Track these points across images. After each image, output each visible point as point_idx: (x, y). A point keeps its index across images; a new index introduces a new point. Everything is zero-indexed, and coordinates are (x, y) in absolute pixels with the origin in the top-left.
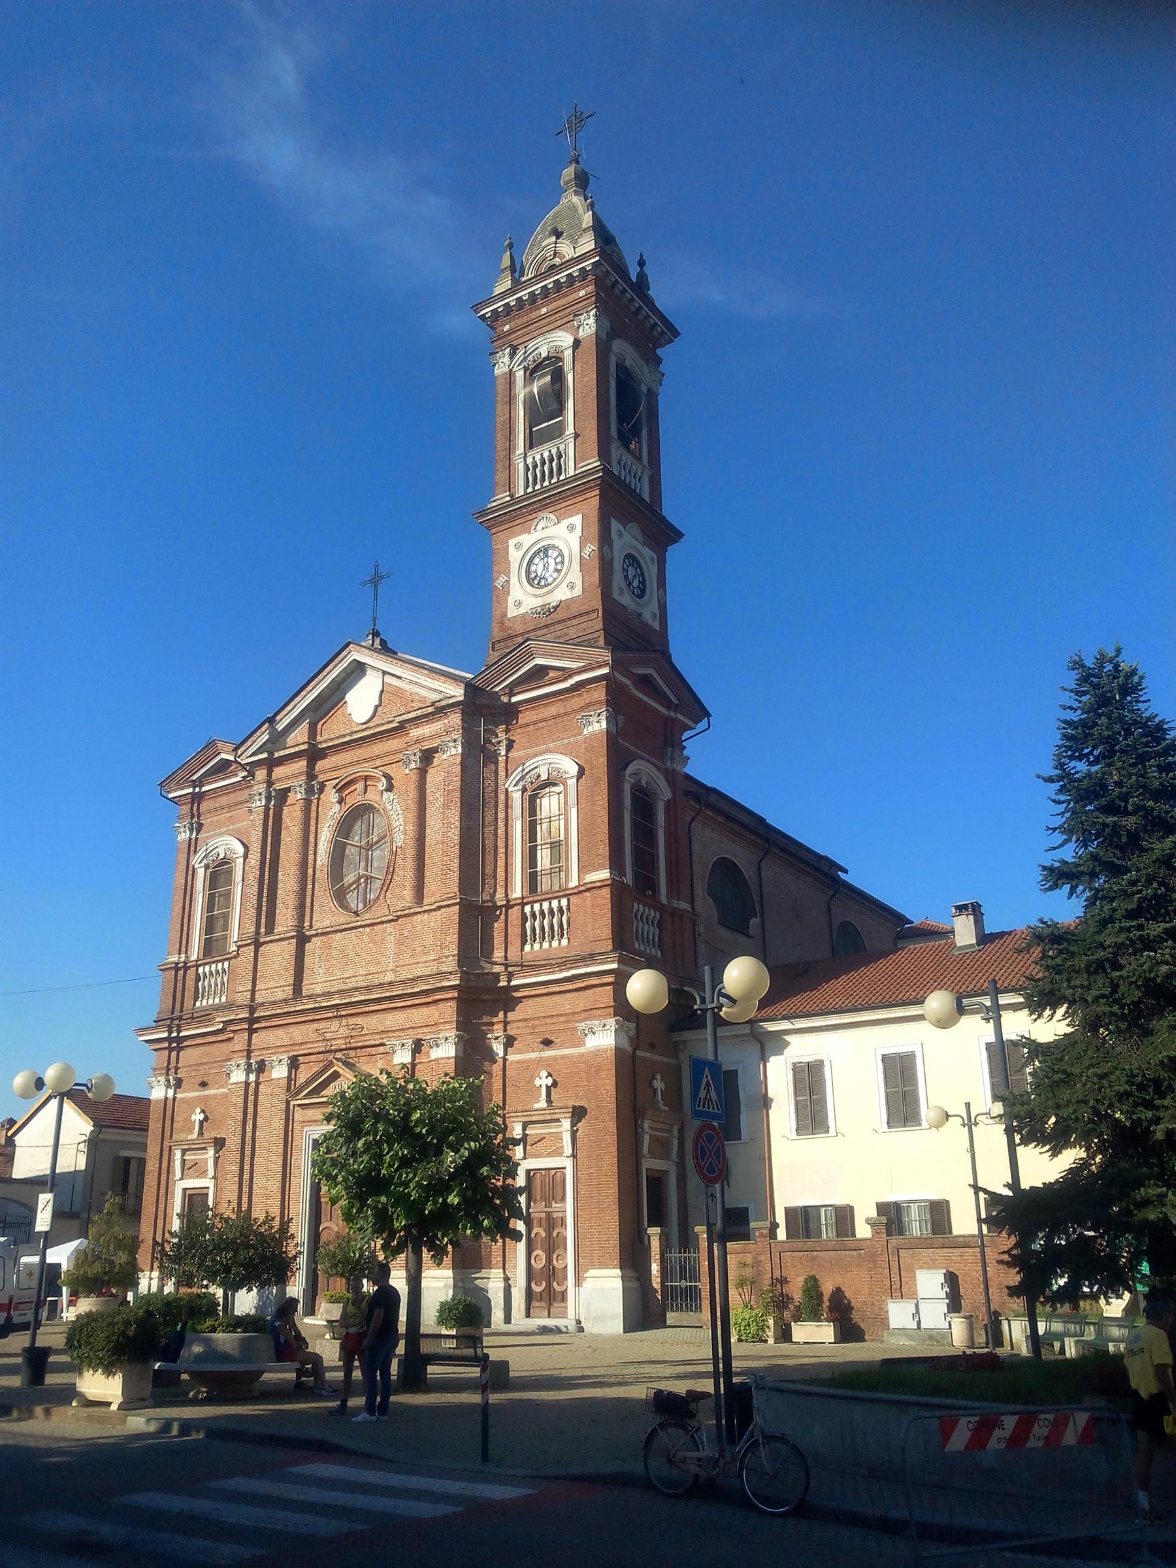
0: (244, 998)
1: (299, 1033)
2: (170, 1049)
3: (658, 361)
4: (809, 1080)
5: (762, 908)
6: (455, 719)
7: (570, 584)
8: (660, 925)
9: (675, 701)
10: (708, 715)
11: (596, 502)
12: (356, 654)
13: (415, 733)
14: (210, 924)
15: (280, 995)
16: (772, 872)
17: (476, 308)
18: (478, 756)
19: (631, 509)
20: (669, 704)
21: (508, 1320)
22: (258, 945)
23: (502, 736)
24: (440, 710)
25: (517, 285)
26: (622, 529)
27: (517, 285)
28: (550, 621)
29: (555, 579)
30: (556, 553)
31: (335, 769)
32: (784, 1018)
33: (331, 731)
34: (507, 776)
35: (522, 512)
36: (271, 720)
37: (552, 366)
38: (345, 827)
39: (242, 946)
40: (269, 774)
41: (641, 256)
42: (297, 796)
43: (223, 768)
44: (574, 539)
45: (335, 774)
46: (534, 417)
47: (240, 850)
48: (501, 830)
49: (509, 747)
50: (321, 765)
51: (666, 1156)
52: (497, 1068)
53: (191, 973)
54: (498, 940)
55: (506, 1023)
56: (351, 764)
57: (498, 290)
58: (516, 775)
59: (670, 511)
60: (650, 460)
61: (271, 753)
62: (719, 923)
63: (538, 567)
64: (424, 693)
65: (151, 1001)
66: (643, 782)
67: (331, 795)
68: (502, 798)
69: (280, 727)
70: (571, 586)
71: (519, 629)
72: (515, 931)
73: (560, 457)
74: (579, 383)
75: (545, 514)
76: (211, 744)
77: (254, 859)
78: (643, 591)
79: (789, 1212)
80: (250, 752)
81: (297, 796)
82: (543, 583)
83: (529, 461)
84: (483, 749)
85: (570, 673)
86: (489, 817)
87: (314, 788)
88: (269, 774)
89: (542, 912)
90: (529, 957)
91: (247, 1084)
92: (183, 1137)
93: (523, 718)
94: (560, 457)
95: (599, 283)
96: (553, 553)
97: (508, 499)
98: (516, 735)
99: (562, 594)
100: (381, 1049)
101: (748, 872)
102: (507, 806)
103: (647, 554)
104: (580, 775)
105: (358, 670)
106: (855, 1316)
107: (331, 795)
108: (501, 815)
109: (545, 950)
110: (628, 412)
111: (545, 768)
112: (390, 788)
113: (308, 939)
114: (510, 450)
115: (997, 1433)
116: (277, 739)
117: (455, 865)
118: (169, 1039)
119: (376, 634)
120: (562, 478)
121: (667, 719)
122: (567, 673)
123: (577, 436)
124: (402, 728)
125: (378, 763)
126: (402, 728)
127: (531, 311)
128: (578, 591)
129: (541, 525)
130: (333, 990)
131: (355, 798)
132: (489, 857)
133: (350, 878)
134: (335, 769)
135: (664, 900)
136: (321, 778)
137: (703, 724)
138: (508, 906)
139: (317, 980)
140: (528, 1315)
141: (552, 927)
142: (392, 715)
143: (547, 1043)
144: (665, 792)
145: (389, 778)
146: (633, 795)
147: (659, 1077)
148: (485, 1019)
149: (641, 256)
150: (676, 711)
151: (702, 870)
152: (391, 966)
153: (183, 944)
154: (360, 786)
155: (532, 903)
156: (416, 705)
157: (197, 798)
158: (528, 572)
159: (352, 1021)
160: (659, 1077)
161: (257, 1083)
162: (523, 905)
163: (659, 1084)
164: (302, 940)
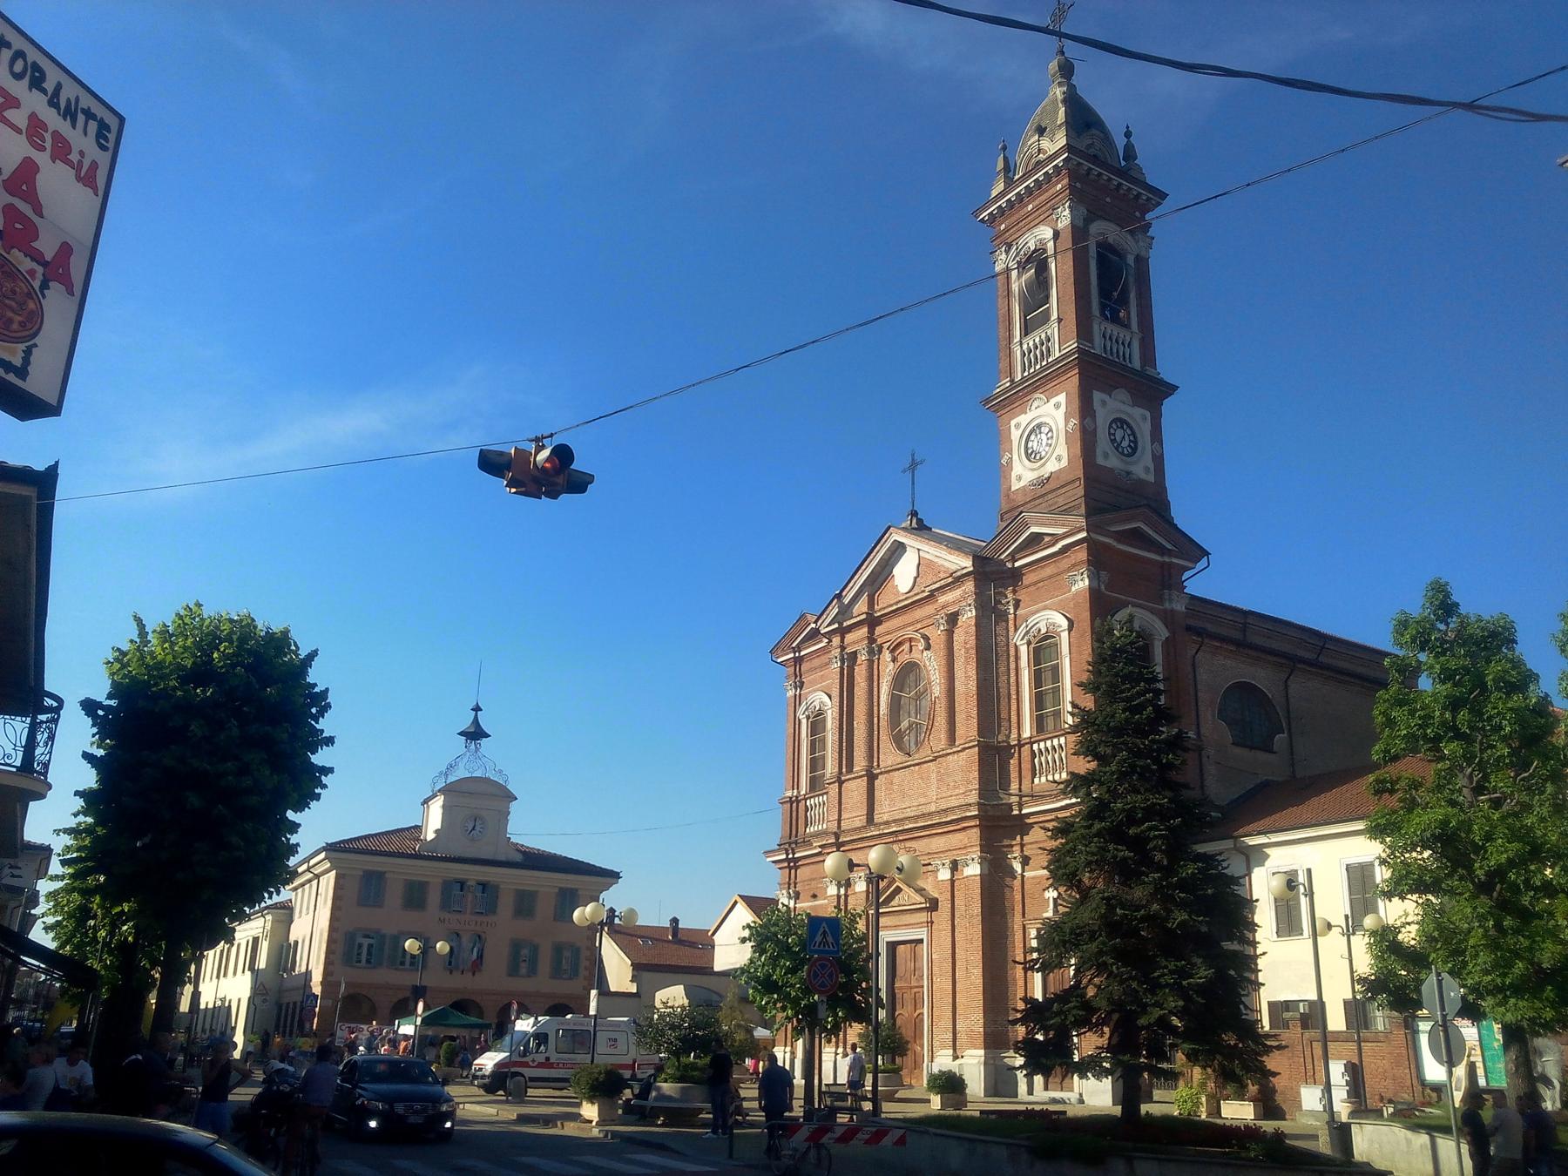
0: (833, 826)
2: (790, 868)
4: (1292, 886)
5: (1289, 724)
6: (969, 586)
7: (1058, 456)
9: (1169, 546)
10: (1208, 554)
11: (1076, 379)
12: (897, 536)
13: (942, 599)
14: (1039, 701)
15: (858, 824)
16: (1304, 688)
17: (976, 213)
18: (991, 617)
19: (1120, 377)
20: (1162, 550)
21: (1030, 1092)
22: (841, 783)
23: (1010, 596)
24: (958, 580)
25: (1010, 183)
27: (1010, 183)
28: (1044, 488)
31: (888, 633)
32: (1260, 833)
33: (885, 602)
34: (1016, 630)
35: (1019, 396)
36: (839, 596)
37: (1036, 259)
38: (900, 681)
40: (842, 641)
42: (863, 657)
43: (815, 634)
44: (1060, 415)
45: (888, 637)
46: (1027, 310)
48: (1013, 680)
49: (1017, 606)
50: (879, 630)
52: (1017, 883)
53: (802, 804)
54: (1014, 775)
55: (1022, 846)
56: (899, 629)
57: (994, 193)
58: (1022, 630)
59: (1165, 369)
60: (1140, 324)
61: (841, 624)
63: (1033, 444)
64: (946, 564)
65: (774, 832)
67: (886, 655)
68: (1012, 652)
69: (846, 601)
70: (1059, 459)
72: (1026, 766)
74: (1060, 271)
75: (1037, 395)
76: (802, 617)
78: (1134, 450)
79: (1273, 1006)
81: (863, 657)
84: (995, 610)
85: (1056, 538)
86: (1002, 669)
87: (874, 650)
88: (842, 641)
90: (1036, 789)
91: (839, 897)
93: (1027, 580)
95: (1074, 175)
96: (1045, 429)
98: (1022, 595)
99: (1052, 466)
102: (1017, 658)
103: (1139, 416)
104: (1070, 629)
105: (899, 549)
106: (1278, 1098)
107: (886, 655)
108: (1012, 666)
110: (1112, 285)
112: (928, 647)
113: (875, 777)
114: (1010, 338)
115: (829, 1135)
116: (845, 611)
117: (974, 712)
118: (787, 860)
119: (914, 514)
121: (1163, 565)
122: (1056, 538)
123: (1060, 320)
124: (932, 595)
126: (932, 595)
127: (1012, 215)
128: (1064, 463)
129: (1035, 404)
131: (904, 658)
132: (1004, 703)
133: (905, 724)
134: (888, 633)
136: (879, 641)
137: (1203, 563)
138: (1020, 745)
139: (883, 812)
140: (1046, 1089)
142: (929, 583)
144: (1161, 632)
145: (926, 638)
148: (1006, 842)
153: (795, 784)
154: (906, 647)
155: (1038, 742)
156: (942, 575)
157: (798, 661)
158: (1026, 448)
159: (908, 844)
161: (846, 896)
162: (1032, 744)
164: (871, 778)
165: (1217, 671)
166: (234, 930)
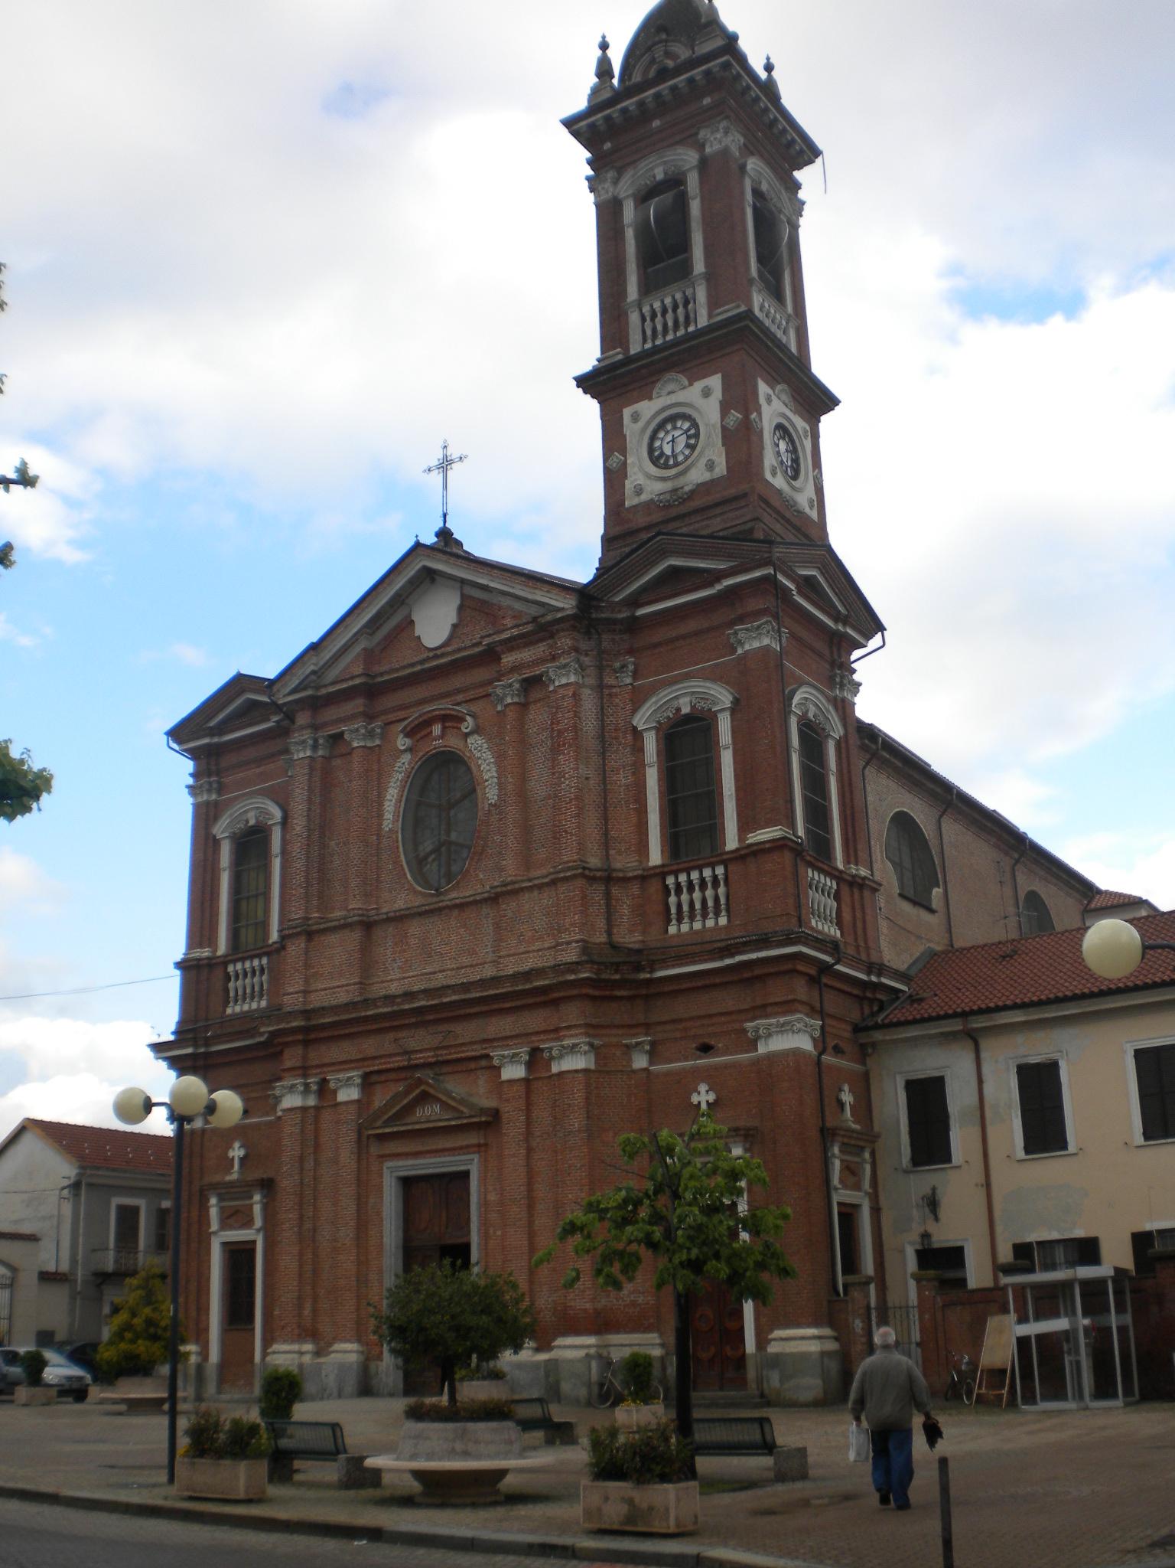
1: (370, 1046)
3: (797, 186)
8: (837, 897)
10: (881, 628)
16: (953, 831)
20: (837, 617)
26: (770, 392)
29: (687, 458)
30: (686, 425)
39: (289, 936)
41: (768, 59)
45: (401, 714)
47: (277, 814)
51: (857, 1187)
62: (900, 895)
66: (811, 715)
71: (642, 520)
73: (686, 302)
75: (672, 375)
77: (299, 824)
80: (288, 690)
82: (671, 462)
83: (646, 309)
85: (719, 576)
89: (703, 881)
92: (217, 1178)
94: (686, 302)
97: (620, 357)
99: (698, 475)
100: (484, 1063)
101: (927, 827)
109: (697, 932)
111: (687, 699)
113: (609, 870)
120: (691, 329)
125: (460, 698)
130: (415, 988)
135: (840, 865)
137: (875, 641)
141: (704, 901)
143: (706, 1049)
144: (837, 730)
146: (801, 732)
147: (846, 1088)
149: (768, 59)
150: (845, 624)
151: (879, 827)
152: (490, 957)
154: (437, 729)
155: (676, 873)
158: (651, 450)
160: (846, 1088)
163: (847, 1097)
165: (885, 798)
166: (186, 1051)
